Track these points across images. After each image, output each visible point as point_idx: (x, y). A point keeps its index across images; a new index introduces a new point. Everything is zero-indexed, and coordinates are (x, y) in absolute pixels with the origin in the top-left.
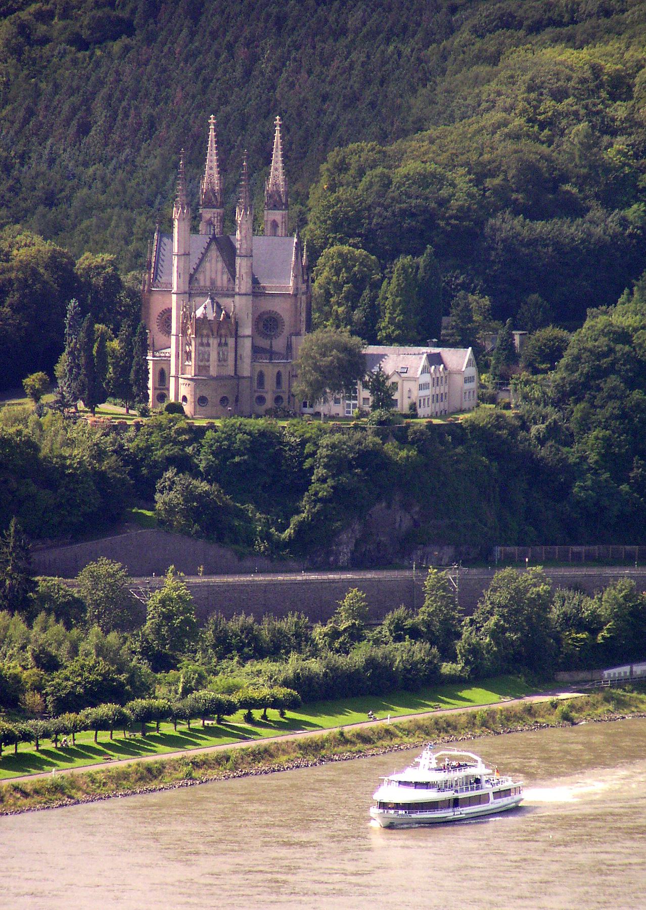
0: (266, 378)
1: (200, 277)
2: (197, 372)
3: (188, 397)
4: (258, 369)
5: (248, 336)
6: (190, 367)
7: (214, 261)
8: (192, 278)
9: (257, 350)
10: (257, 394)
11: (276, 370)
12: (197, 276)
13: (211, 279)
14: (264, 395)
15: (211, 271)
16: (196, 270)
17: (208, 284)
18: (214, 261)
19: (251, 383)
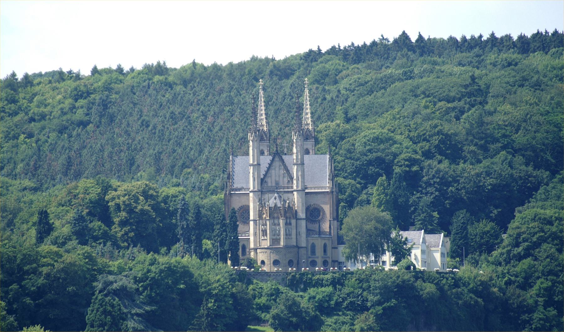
0: (317, 248)
1: (268, 180)
2: (271, 244)
3: (266, 261)
4: (311, 242)
5: (304, 219)
6: (265, 241)
7: (277, 169)
8: (263, 181)
9: (309, 231)
10: (310, 260)
11: (323, 242)
12: (266, 179)
13: (276, 181)
14: (316, 259)
15: (276, 176)
16: (265, 176)
17: (274, 185)
18: (277, 169)
19: (307, 252)
